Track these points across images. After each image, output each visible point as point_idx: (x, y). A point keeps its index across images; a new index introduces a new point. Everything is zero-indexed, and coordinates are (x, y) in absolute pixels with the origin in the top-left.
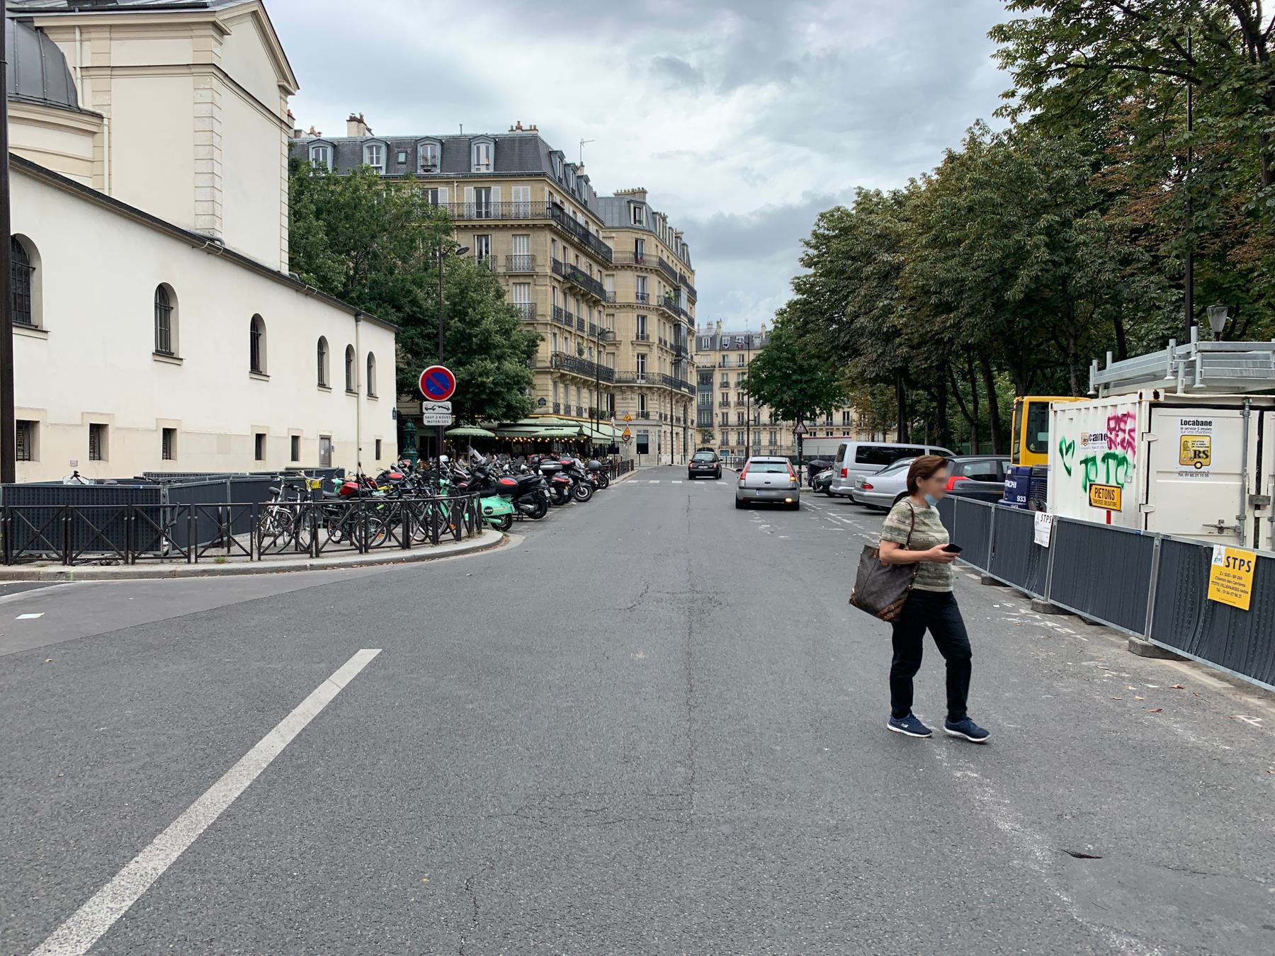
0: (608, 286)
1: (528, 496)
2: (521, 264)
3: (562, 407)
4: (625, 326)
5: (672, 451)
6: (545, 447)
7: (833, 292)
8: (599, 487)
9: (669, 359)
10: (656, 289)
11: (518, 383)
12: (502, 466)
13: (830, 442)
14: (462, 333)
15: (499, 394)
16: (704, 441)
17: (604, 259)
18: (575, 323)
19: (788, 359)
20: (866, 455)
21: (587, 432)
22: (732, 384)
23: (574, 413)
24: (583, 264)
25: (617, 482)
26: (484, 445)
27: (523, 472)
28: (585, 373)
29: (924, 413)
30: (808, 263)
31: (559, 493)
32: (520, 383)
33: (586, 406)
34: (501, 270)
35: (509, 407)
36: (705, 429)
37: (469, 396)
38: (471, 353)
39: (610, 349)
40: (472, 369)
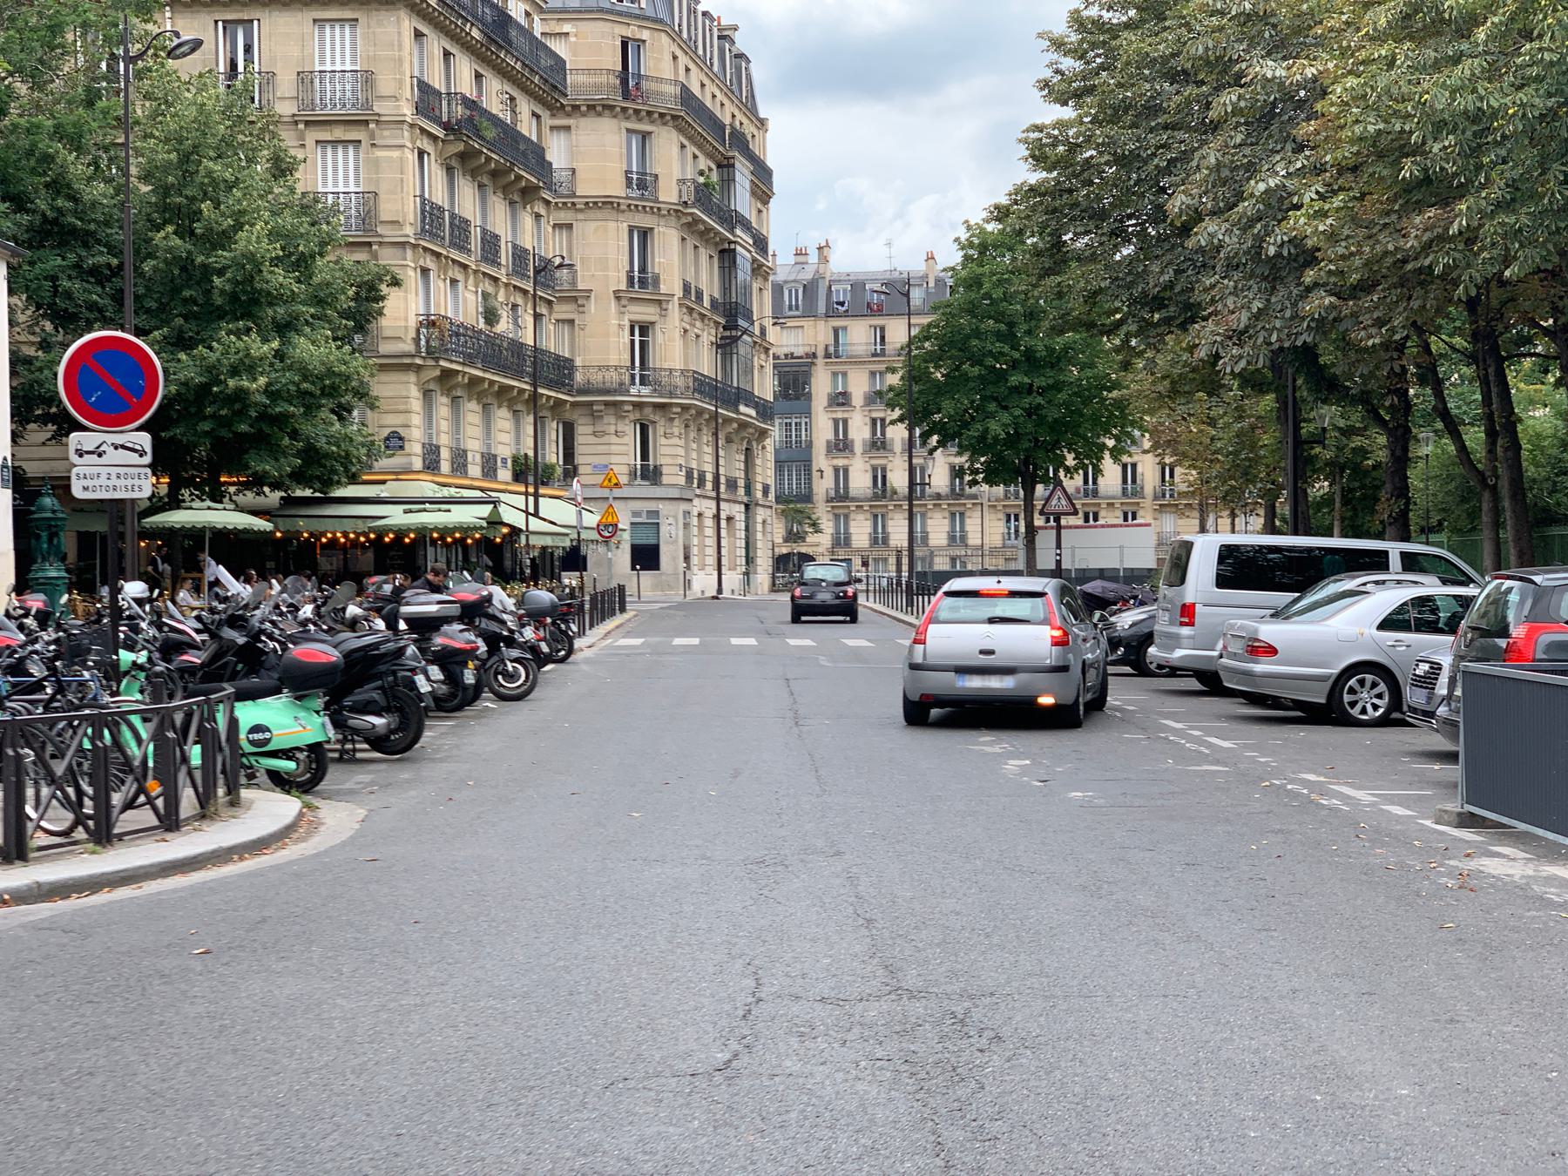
0: (557, 153)
1: (369, 692)
2: (337, 95)
3: (445, 454)
4: (600, 254)
5: (714, 558)
6: (404, 555)
7: (1121, 161)
8: (549, 659)
9: (708, 336)
10: (675, 164)
11: (332, 392)
12: (295, 609)
13: (1129, 535)
14: (186, 265)
15: (281, 420)
16: (792, 537)
17: (547, 85)
18: (475, 242)
19: (999, 336)
20: (1240, 569)
21: (512, 517)
22: (858, 399)
23: (475, 470)
24: (494, 96)
25: (592, 642)
26: (242, 553)
27: (353, 624)
28: (503, 369)
29: (1329, 463)
30: (1059, 92)
31: (453, 678)
32: (335, 392)
33: (504, 451)
34: (286, 109)
35: (311, 455)
36: (796, 506)
37: (206, 426)
38: (210, 315)
39: (563, 311)
40: (213, 357)
